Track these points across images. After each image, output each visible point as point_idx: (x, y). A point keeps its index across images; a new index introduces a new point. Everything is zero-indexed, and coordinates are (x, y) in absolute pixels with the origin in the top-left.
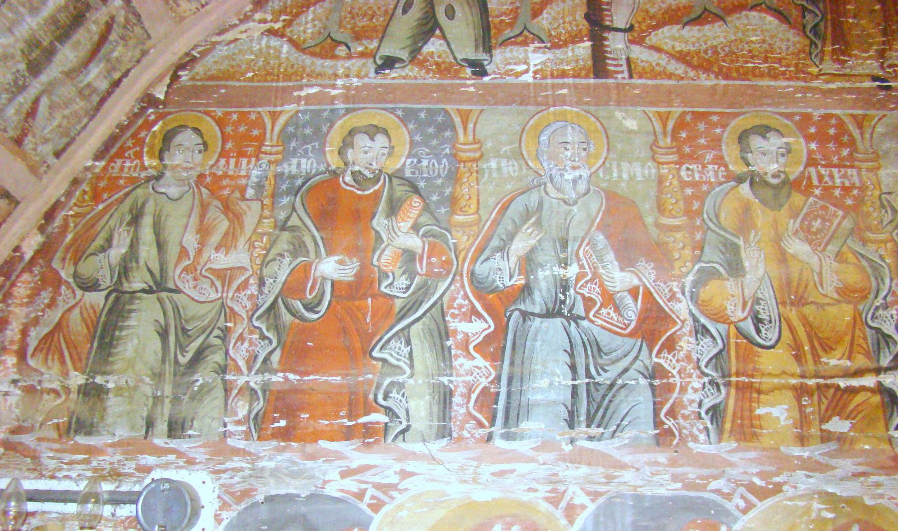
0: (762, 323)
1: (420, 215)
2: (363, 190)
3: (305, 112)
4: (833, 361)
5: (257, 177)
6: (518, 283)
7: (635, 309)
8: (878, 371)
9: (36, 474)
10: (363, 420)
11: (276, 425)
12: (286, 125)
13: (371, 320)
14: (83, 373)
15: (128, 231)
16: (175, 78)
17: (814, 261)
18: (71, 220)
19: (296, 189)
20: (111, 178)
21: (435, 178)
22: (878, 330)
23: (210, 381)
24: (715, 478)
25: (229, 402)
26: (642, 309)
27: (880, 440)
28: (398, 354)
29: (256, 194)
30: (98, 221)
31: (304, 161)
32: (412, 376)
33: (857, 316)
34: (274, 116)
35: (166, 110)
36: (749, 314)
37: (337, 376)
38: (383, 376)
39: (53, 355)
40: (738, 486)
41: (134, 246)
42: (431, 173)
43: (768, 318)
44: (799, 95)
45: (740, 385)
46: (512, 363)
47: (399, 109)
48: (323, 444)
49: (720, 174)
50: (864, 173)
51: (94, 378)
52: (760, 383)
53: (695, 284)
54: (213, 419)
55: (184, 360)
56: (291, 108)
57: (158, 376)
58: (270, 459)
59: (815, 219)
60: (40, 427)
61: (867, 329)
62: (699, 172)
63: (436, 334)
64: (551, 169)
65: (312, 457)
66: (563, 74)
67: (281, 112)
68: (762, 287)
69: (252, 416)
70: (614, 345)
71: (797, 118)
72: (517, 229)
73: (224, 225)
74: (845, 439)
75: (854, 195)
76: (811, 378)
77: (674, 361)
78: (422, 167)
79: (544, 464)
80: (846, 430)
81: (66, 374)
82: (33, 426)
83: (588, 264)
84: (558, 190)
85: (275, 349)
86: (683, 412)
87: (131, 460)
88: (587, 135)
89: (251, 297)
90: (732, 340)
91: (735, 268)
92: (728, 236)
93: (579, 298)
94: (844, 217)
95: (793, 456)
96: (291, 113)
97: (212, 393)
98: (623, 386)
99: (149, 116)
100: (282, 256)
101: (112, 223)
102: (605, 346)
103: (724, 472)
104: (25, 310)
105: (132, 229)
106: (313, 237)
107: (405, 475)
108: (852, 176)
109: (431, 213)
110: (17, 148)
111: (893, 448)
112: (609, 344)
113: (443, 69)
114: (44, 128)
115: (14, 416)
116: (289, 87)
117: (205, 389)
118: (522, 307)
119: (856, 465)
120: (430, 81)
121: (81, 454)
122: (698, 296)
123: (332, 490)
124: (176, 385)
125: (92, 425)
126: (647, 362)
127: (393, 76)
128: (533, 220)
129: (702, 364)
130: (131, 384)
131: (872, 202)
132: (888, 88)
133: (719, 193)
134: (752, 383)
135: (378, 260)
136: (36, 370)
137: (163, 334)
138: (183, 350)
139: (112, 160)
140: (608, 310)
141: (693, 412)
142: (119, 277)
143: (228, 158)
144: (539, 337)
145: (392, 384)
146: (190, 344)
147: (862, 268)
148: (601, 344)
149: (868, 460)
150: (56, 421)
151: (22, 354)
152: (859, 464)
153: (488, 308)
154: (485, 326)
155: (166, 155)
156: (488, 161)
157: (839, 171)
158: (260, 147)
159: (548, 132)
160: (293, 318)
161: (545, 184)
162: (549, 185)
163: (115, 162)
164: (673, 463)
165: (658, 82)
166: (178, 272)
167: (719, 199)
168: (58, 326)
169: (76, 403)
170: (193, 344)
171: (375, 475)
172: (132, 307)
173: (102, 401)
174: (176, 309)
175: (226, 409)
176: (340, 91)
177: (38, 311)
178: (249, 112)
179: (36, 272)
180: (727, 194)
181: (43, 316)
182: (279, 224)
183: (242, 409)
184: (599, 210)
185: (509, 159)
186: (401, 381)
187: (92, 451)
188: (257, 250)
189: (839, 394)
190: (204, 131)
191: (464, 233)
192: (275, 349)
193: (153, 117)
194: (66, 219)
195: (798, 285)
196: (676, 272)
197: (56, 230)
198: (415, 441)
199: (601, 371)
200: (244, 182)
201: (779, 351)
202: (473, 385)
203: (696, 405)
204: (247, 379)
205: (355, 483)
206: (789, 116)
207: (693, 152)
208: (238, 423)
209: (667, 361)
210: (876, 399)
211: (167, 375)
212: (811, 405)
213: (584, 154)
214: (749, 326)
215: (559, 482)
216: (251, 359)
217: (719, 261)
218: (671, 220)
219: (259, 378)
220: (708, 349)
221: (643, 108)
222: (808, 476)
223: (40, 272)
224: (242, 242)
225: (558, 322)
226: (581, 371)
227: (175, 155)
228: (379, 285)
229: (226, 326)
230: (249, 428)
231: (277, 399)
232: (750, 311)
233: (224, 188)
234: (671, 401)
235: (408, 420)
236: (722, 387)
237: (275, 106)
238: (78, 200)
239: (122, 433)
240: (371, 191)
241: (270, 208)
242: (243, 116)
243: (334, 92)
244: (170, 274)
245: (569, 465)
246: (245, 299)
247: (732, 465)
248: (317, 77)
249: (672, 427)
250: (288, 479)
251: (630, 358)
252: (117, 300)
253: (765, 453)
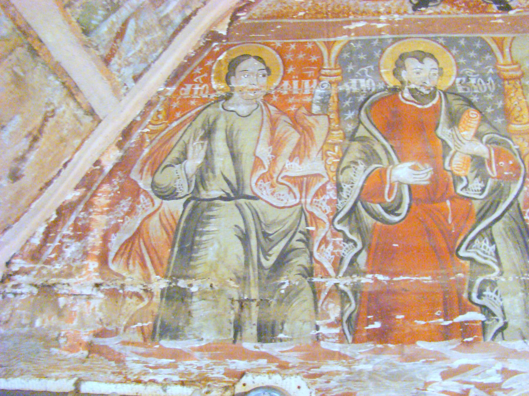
1: (479, 126)
2: (423, 104)
3: (356, 41)
5: (321, 95)
9: (121, 378)
10: (460, 318)
11: (371, 327)
12: (341, 52)
13: (453, 220)
14: (166, 277)
15: (202, 145)
18: (146, 136)
19: (359, 105)
20: (182, 100)
21: (485, 94)
23: (297, 283)
25: (320, 304)
28: (484, 252)
29: (322, 109)
30: (172, 137)
31: (362, 81)
32: (501, 274)
34: (329, 46)
35: (229, 43)
37: (427, 275)
38: (474, 275)
39: (134, 260)
41: (209, 157)
42: (481, 89)
47: (440, 37)
48: (421, 344)
51: (177, 282)
54: (305, 322)
55: (268, 263)
56: (343, 39)
58: (367, 363)
60: (125, 331)
63: (517, 232)
65: (412, 358)
67: (334, 42)
69: (345, 318)
73: (294, 137)
78: (471, 84)
81: (147, 278)
82: (117, 329)
85: (360, 252)
87: (219, 364)
89: (330, 202)
96: (345, 43)
97: (300, 295)
99: (214, 48)
100: (356, 163)
101: (186, 138)
104: (106, 217)
105: (206, 142)
106: (383, 146)
107: (506, 373)
109: (489, 123)
110: (104, 67)
114: (129, 51)
115: (98, 319)
116: (338, 22)
117: (293, 292)
120: (462, 16)
121: (167, 358)
124: (262, 288)
125: (177, 329)
130: (216, 288)
135: (450, 164)
136: (117, 274)
137: (244, 239)
138: (266, 254)
139: (182, 85)
142: (196, 186)
143: (291, 80)
145: (484, 282)
146: (272, 247)
150: (140, 324)
151: (103, 260)
155: (232, 79)
158: (319, 71)
160: (374, 221)
163: (185, 87)
166: (254, 180)
168: (138, 232)
169: (160, 307)
170: (275, 248)
171: (477, 374)
172: (211, 213)
173: (187, 305)
174: (256, 214)
175: (316, 312)
176: (385, 25)
177: (118, 218)
178: (305, 43)
179: (115, 183)
181: (123, 223)
182: (349, 135)
186: (493, 279)
187: (177, 355)
188: (331, 158)
190: (265, 59)
191: (524, 140)
192: (360, 252)
193: (217, 49)
194: (142, 136)
197: (133, 146)
198: (514, 339)
200: (308, 99)
204: (336, 281)
205: (456, 383)
208: (331, 325)
211: (252, 278)
216: (338, 261)
219: (348, 281)
223: (119, 183)
224: (314, 152)
227: (241, 79)
228: (455, 188)
229: (308, 230)
230: (343, 330)
231: (369, 301)
233: (291, 105)
235: (504, 318)
237: (328, 37)
238: (153, 119)
240: (430, 105)
241: (337, 121)
242: (301, 47)
243: (379, 26)
244: (247, 181)
246: (324, 203)
248: (361, 15)
250: (387, 382)
252: (195, 207)
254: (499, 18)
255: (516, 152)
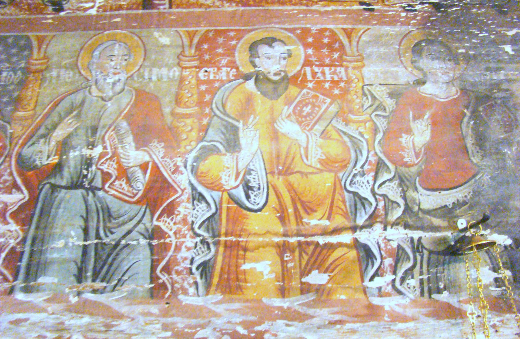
0: (252, 190)
6: (53, 162)
7: (143, 181)
8: (354, 229)
17: (302, 138)
21: (9, 85)
22: (355, 194)
24: (203, 327)
26: (150, 181)
27: (356, 290)
33: (337, 182)
36: (240, 183)
40: (223, 334)
42: (7, 81)
43: (257, 186)
44: (301, 16)
45: (228, 243)
46: (37, 228)
49: (231, 74)
50: (350, 71)
52: (247, 242)
53: (197, 159)
59: (307, 105)
61: (346, 194)
62: (214, 73)
64: (97, 76)
68: (254, 160)
70: (122, 211)
71: (299, 32)
72: (61, 119)
74: (324, 290)
75: (341, 87)
76: (292, 236)
77: (172, 224)
79: (53, 314)
80: (324, 282)
83: (111, 145)
84: (100, 90)
86: (176, 268)
88: (129, 50)
90: (225, 205)
92: (231, 121)
93: (99, 173)
94: (331, 104)
95: (274, 307)
98: (127, 245)
102: (114, 212)
103: (210, 321)
108: (340, 72)
111: (367, 298)
112: (118, 210)
118: (52, 181)
119: (333, 314)
120: (21, 17)
122: (198, 169)
126: (148, 225)
128: (74, 113)
129: (196, 226)
131: (356, 92)
132: (372, 10)
133: (228, 88)
134: (239, 242)
140: (120, 182)
141: (186, 268)
144: (62, 206)
147: (344, 143)
148: (113, 210)
152: (337, 313)
153: (27, 183)
154: (21, 196)
156: (51, 70)
157: (330, 69)
159: (101, 48)
161: (91, 86)
162: (94, 87)
164: (165, 313)
165: (191, 10)
167: (227, 93)
174: (291, 188)
180: (234, 89)
184: (128, 105)
185: (67, 68)
189: (318, 250)
191: (21, 125)
195: (286, 157)
196: (182, 150)
199: (108, 233)
201: (265, 213)
202: (4, 246)
203: (188, 262)
206: (292, 31)
207: (211, 59)
210: (353, 254)
212: (292, 261)
213: (124, 63)
214: (240, 193)
215: (65, 329)
217: (219, 139)
218: (186, 109)
221: (176, 29)
222: (287, 325)
225: (79, 192)
226: (92, 233)
232: (242, 180)
234: (167, 259)
236: (212, 246)
245: (74, 315)
247: (217, 315)
249: (166, 281)
251: (135, 221)
253: (248, 304)
254: (49, 17)
255: (9, 135)
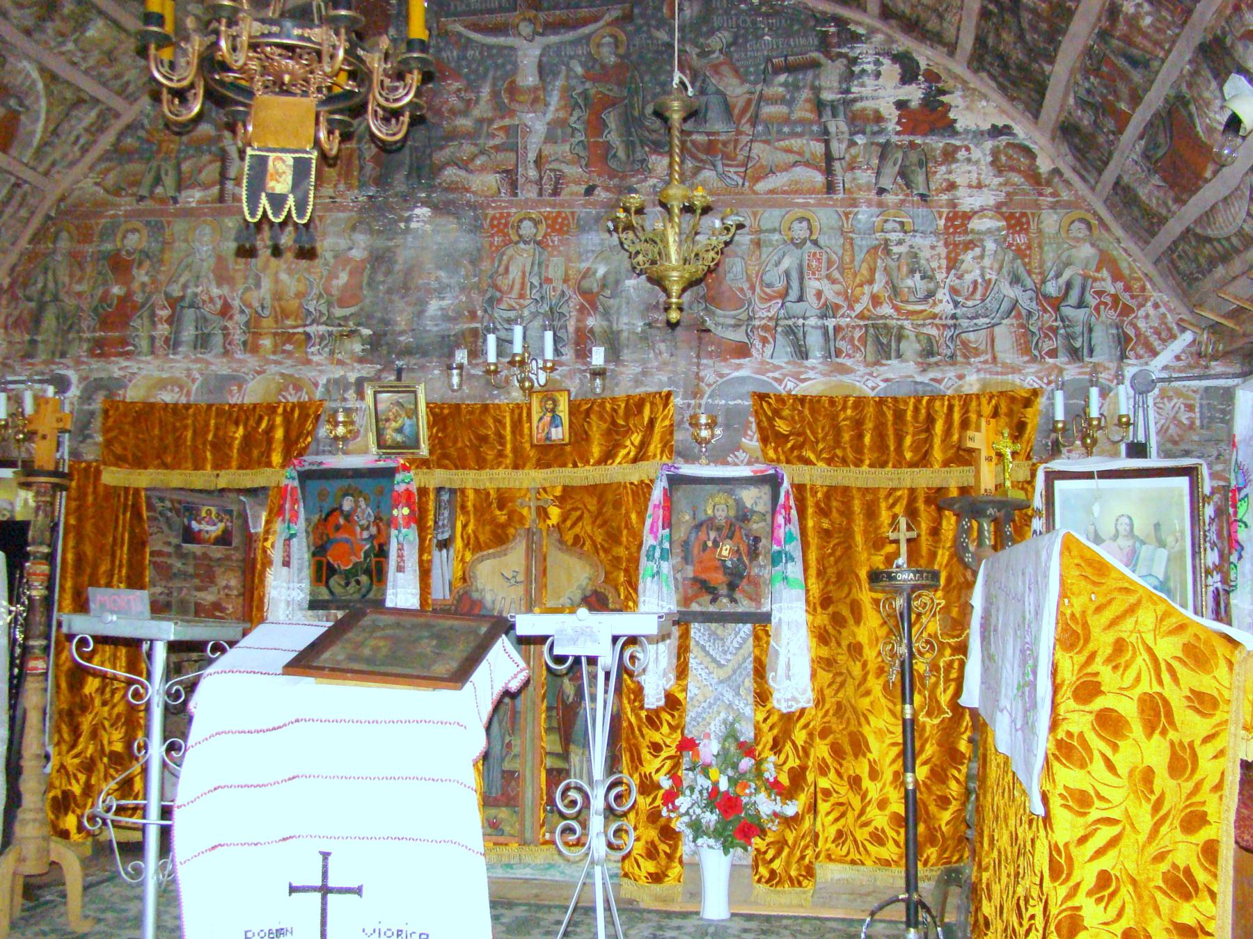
4: (289, 322)
8: (305, 326)
16: (58, 206)
56: (103, 221)
57: (56, 335)
66: (207, 202)
73: (78, 274)
91: (258, 285)
113: (163, 201)
123: (116, 375)
127: (142, 205)
137: (57, 319)
149: (998, 514)
153: (171, 306)
174: (280, 306)
183: (85, 346)
187: (32, 364)
209: (229, 324)
214: (259, 310)
216: (89, 328)
220: (244, 319)
239: (44, 357)
